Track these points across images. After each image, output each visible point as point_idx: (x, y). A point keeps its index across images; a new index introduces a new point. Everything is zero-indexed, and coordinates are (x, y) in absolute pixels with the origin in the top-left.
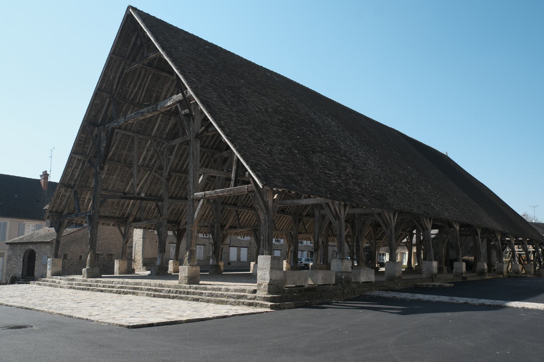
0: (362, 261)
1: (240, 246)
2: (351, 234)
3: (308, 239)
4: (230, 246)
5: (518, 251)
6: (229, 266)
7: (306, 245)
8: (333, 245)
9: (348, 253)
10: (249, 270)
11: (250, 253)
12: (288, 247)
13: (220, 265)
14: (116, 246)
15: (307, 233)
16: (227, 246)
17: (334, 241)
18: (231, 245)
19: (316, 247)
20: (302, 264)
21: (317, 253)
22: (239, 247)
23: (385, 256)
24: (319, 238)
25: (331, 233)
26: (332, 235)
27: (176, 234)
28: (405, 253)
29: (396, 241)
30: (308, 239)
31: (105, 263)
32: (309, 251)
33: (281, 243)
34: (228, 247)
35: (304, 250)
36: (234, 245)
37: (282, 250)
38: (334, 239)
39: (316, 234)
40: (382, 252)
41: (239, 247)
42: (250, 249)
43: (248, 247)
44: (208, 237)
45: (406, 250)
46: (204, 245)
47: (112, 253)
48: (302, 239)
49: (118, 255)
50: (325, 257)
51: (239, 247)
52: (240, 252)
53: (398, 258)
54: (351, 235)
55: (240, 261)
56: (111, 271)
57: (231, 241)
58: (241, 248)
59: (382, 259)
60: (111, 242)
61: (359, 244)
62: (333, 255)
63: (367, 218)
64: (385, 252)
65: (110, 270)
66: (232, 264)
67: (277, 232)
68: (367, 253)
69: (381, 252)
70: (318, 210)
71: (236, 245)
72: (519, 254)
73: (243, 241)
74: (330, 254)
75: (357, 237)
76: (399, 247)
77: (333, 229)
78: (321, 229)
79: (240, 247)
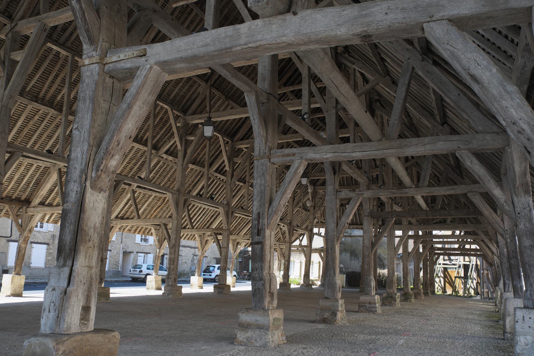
0: (272, 294)
2: (224, 226)
3: (146, 233)
4: (9, 241)
5: (444, 264)
8: (194, 246)
9: (214, 258)
11: (51, 253)
15: (139, 217)
17: (193, 238)
19: (68, 238)
20: (141, 273)
21: (67, 270)
24: (89, 190)
25: (189, 224)
26: (190, 227)
30: (146, 233)
34: (6, 241)
35: (149, 252)
37: (112, 251)
38: (150, 230)
39: (77, 167)
42: (52, 247)
43: (48, 244)
48: (135, 231)
50: (172, 266)
52: (31, 251)
54: (224, 228)
58: (34, 245)
61: (264, 237)
62: (194, 261)
63: (294, 155)
68: (240, 260)
70: (95, 50)
72: (444, 268)
73: (39, 232)
75: (259, 214)
77: (193, 217)
78: (104, 144)
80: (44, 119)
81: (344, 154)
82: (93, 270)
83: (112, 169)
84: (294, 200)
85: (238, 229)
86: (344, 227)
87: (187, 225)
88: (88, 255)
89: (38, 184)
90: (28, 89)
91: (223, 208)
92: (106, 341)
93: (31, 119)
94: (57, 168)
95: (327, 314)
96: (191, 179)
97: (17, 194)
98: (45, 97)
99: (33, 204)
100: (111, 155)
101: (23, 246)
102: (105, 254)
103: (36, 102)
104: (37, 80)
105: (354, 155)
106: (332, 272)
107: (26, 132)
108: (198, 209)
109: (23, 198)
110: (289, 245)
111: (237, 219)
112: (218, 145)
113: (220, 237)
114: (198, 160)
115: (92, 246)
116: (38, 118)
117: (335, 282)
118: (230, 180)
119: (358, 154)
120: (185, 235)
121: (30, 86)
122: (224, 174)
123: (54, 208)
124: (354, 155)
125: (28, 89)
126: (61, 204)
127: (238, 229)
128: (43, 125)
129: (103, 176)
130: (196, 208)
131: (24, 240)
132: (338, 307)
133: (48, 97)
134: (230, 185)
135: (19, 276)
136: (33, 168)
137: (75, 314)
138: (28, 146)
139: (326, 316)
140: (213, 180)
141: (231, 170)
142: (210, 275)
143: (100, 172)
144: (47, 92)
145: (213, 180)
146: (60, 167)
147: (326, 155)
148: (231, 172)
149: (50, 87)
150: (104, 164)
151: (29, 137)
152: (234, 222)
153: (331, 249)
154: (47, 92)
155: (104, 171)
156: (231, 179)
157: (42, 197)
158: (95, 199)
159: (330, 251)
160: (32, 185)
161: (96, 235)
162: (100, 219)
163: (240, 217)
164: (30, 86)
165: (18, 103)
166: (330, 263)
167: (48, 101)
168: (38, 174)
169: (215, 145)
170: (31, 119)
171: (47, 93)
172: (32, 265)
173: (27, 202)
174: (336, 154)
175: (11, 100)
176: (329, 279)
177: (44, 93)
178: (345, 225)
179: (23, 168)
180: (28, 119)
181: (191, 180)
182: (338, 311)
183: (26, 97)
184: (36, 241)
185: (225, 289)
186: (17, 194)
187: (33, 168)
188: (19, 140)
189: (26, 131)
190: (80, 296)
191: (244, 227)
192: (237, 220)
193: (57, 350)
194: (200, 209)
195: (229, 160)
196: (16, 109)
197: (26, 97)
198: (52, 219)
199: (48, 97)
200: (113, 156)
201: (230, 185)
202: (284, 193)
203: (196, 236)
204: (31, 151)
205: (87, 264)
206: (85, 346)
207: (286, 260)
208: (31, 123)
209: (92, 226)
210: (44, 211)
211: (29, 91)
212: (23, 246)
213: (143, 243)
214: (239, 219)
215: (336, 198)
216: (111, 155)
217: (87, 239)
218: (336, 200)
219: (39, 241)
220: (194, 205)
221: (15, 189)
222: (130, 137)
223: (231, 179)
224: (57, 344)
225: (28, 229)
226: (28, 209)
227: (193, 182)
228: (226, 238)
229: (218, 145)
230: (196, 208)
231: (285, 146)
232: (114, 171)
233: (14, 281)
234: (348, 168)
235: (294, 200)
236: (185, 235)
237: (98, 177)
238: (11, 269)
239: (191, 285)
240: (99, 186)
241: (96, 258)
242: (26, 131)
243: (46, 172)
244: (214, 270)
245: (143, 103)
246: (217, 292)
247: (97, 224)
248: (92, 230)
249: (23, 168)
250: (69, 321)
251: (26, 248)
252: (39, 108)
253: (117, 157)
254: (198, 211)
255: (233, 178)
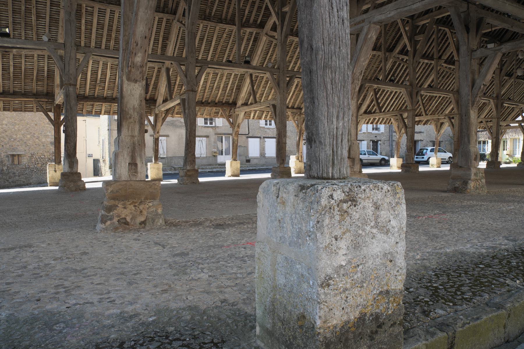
1: (265, 136)
4: (248, 137)
6: (248, 164)
7: (366, 131)
9: (430, 141)
10: (223, 173)
12: (298, 133)
13: (80, 173)
14: (25, 143)
16: (244, 137)
18: (250, 135)
22: (262, 137)
23: (486, 146)
26: (378, 111)
27: (53, 118)
28: (519, 139)
29: (478, 117)
31: (5, 168)
32: (371, 140)
33: (381, 131)
34: (245, 138)
36: (255, 136)
38: (391, 120)
40: (483, 139)
41: (262, 138)
44: (213, 125)
45: (521, 135)
46: (207, 137)
47: (19, 153)
49: (30, 155)
51: (262, 137)
53: (508, 147)
55: (264, 157)
56: (17, 180)
57: (250, 130)
58: (266, 139)
59: (483, 149)
60: (15, 136)
64: (487, 139)
65: (17, 178)
66: (253, 162)
67: (256, 106)
69: (482, 139)
71: (257, 136)
73: (269, 129)
74: (403, 144)
76: (508, 131)
79: (264, 138)
80: (231, 35)
81: (406, 9)
82: (136, 138)
83: (139, 64)
84: (501, 70)
85: (440, 109)
86: (479, 89)
87: (376, 110)
88: (130, 128)
89: (239, 89)
90: (213, 14)
91: (405, 88)
92: (148, 187)
93: (221, 38)
94: (249, 73)
95: (458, 183)
96: (375, 65)
97: (225, 99)
98: (227, 17)
99: (238, 105)
100: (134, 54)
101: (236, 138)
102: (284, 139)
103: (221, 23)
104: (218, 5)
105: (414, 6)
106: (466, 140)
107: (220, 49)
108: (388, 93)
109: (231, 101)
110: (496, 121)
111: (436, 99)
112: (397, 28)
113: (453, 120)
114: (378, 45)
115: (133, 121)
116: (226, 35)
117: (469, 150)
118: (412, 60)
119: (418, 5)
120: (381, 120)
121: (214, 10)
122: (406, 53)
123: (250, 106)
124: (414, 6)
125: (213, 14)
126: (169, 98)
127: (440, 109)
128: (231, 40)
129: (133, 70)
130: (387, 92)
131: (236, 134)
132: (470, 175)
133: (229, 17)
134: (413, 64)
135: (235, 162)
136: (232, 76)
137: (123, 167)
138: (209, 59)
139: (457, 185)
140: (400, 64)
141: (412, 49)
142: (423, 158)
143: (130, 68)
144: (227, 12)
145: (400, 64)
146: (251, 73)
147: (390, 13)
148: (412, 51)
149: (228, 8)
150: (130, 61)
151: (223, 52)
152: (434, 103)
153: (465, 116)
154: (227, 12)
155: (132, 66)
156: (413, 58)
157: (245, 99)
158: (132, 88)
159: (464, 117)
160: (234, 90)
161: (136, 114)
162: (138, 102)
163: (440, 97)
164: (214, 10)
165: (209, 27)
166: (464, 130)
167: (230, 20)
168: (237, 81)
169: (394, 27)
170: (221, 38)
171: (228, 13)
172: (266, 155)
173: (234, 104)
174: (399, 10)
175: (193, 26)
176: (464, 147)
177: (231, 13)
178: (480, 87)
179: (225, 78)
180: (219, 38)
181: (375, 66)
182: (470, 179)
183: (213, 21)
184: (267, 136)
185: (412, 168)
186: (225, 99)
187: (232, 76)
188: (217, 56)
189: (220, 48)
190: (125, 156)
191: (447, 107)
192: (438, 100)
193: (107, 190)
194: (391, 93)
195: (410, 39)
196: (209, 32)
197: (213, 21)
198: (256, 116)
199: (229, 17)
200: (135, 54)
201: (413, 64)
202: (356, 61)
203: (392, 119)
204: (212, 62)
205: (130, 134)
206: (129, 189)
207: (493, 137)
208: (222, 40)
209: (132, 107)
210: (244, 110)
211: (214, 15)
212: (236, 138)
213: (375, 132)
214: (439, 99)
215: (471, 58)
216: (134, 54)
217: (128, 116)
218: (471, 60)
219: (270, 136)
220: (383, 91)
221: (223, 95)
222: (146, 37)
223: (413, 58)
224: (106, 186)
225: (237, 125)
226: (235, 110)
227: (378, 68)
228: (411, 118)
229: (397, 28)
230: (387, 92)
231: (495, 11)
232: (141, 65)
233: (233, 165)
234: (286, 24)
235: (501, 70)
236: (381, 120)
237: (130, 71)
238: (252, 159)
239: (391, 167)
240: (133, 78)
241: (138, 130)
242: (220, 48)
243: (242, 78)
244: (426, 153)
245: (146, 9)
246: (404, 171)
247: (136, 106)
248: (132, 110)
249: (225, 78)
250: (119, 172)
251: (238, 140)
252: (224, 27)
253: (140, 54)
254: (389, 96)
255: (415, 58)
